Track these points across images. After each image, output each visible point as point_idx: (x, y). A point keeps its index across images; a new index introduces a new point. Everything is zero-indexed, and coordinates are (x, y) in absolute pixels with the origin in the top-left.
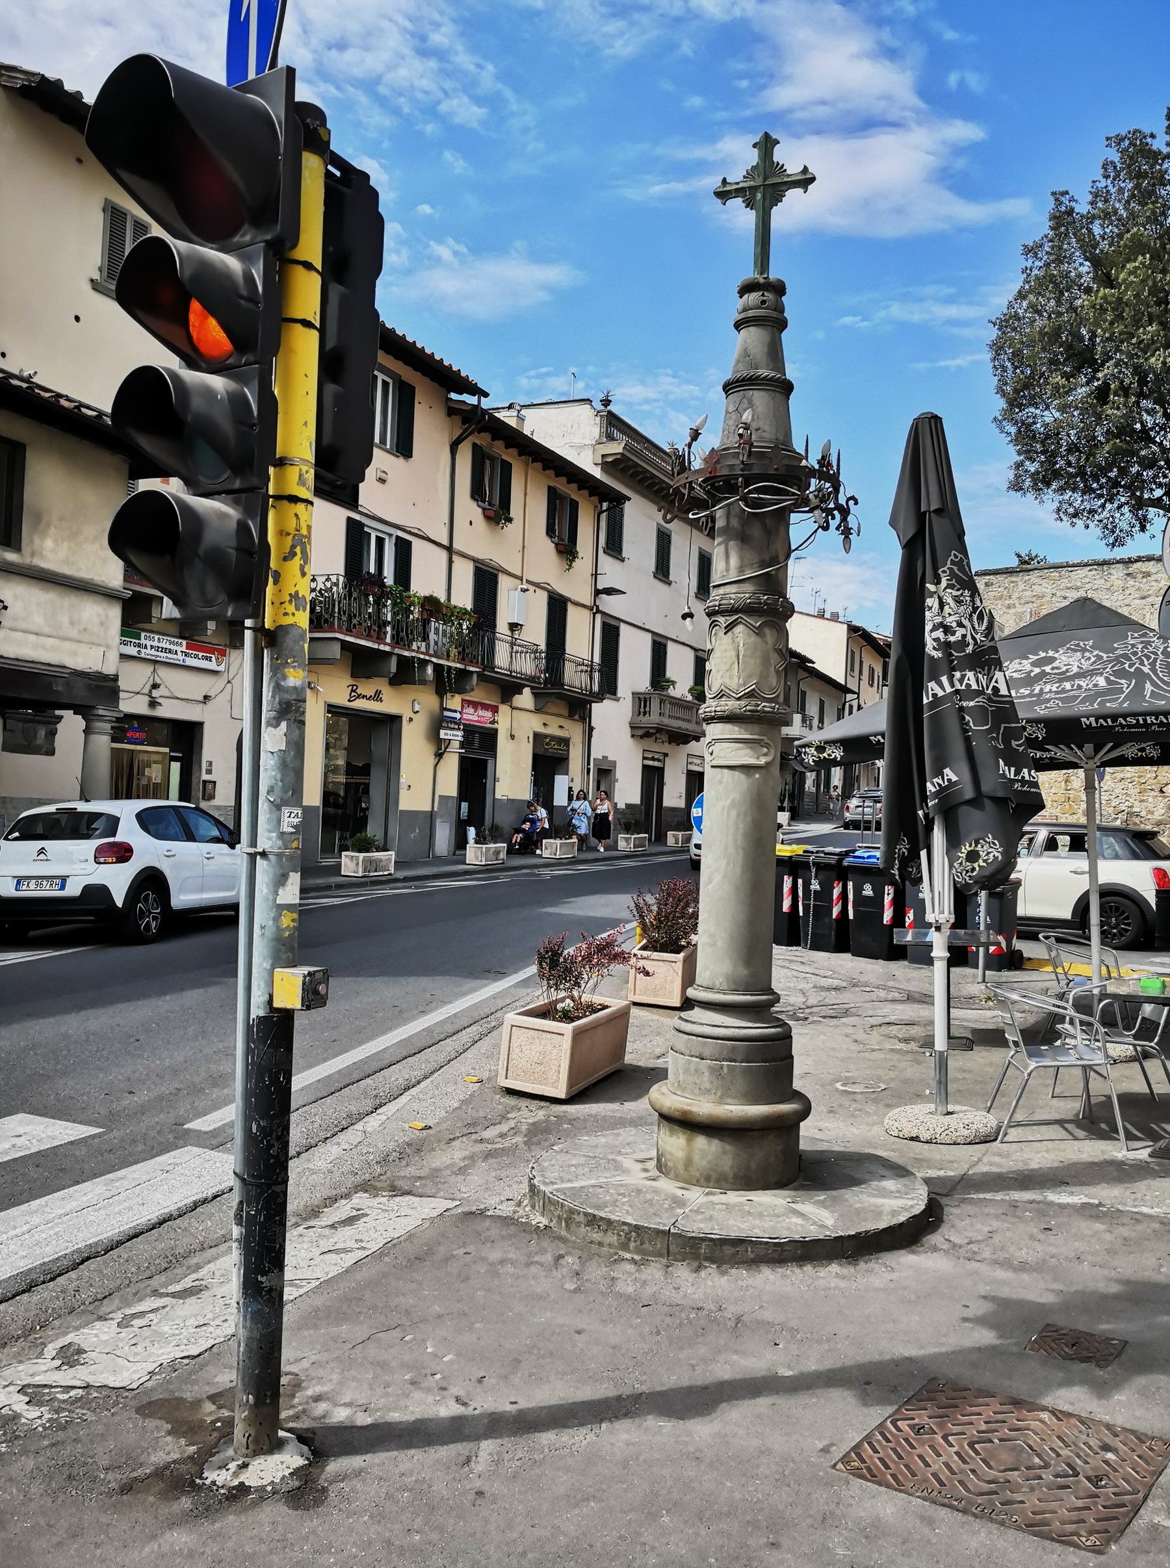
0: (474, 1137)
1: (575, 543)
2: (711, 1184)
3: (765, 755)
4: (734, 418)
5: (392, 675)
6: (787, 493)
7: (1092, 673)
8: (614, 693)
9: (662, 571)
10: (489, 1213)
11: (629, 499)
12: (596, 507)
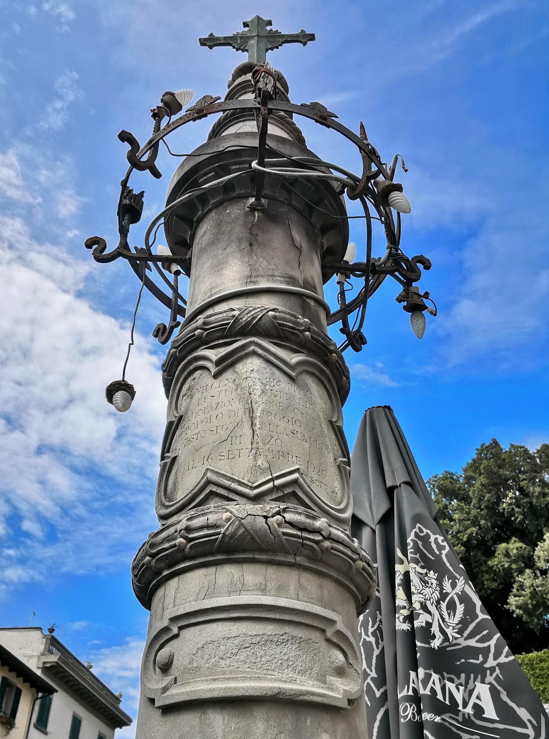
12: (33, 695)
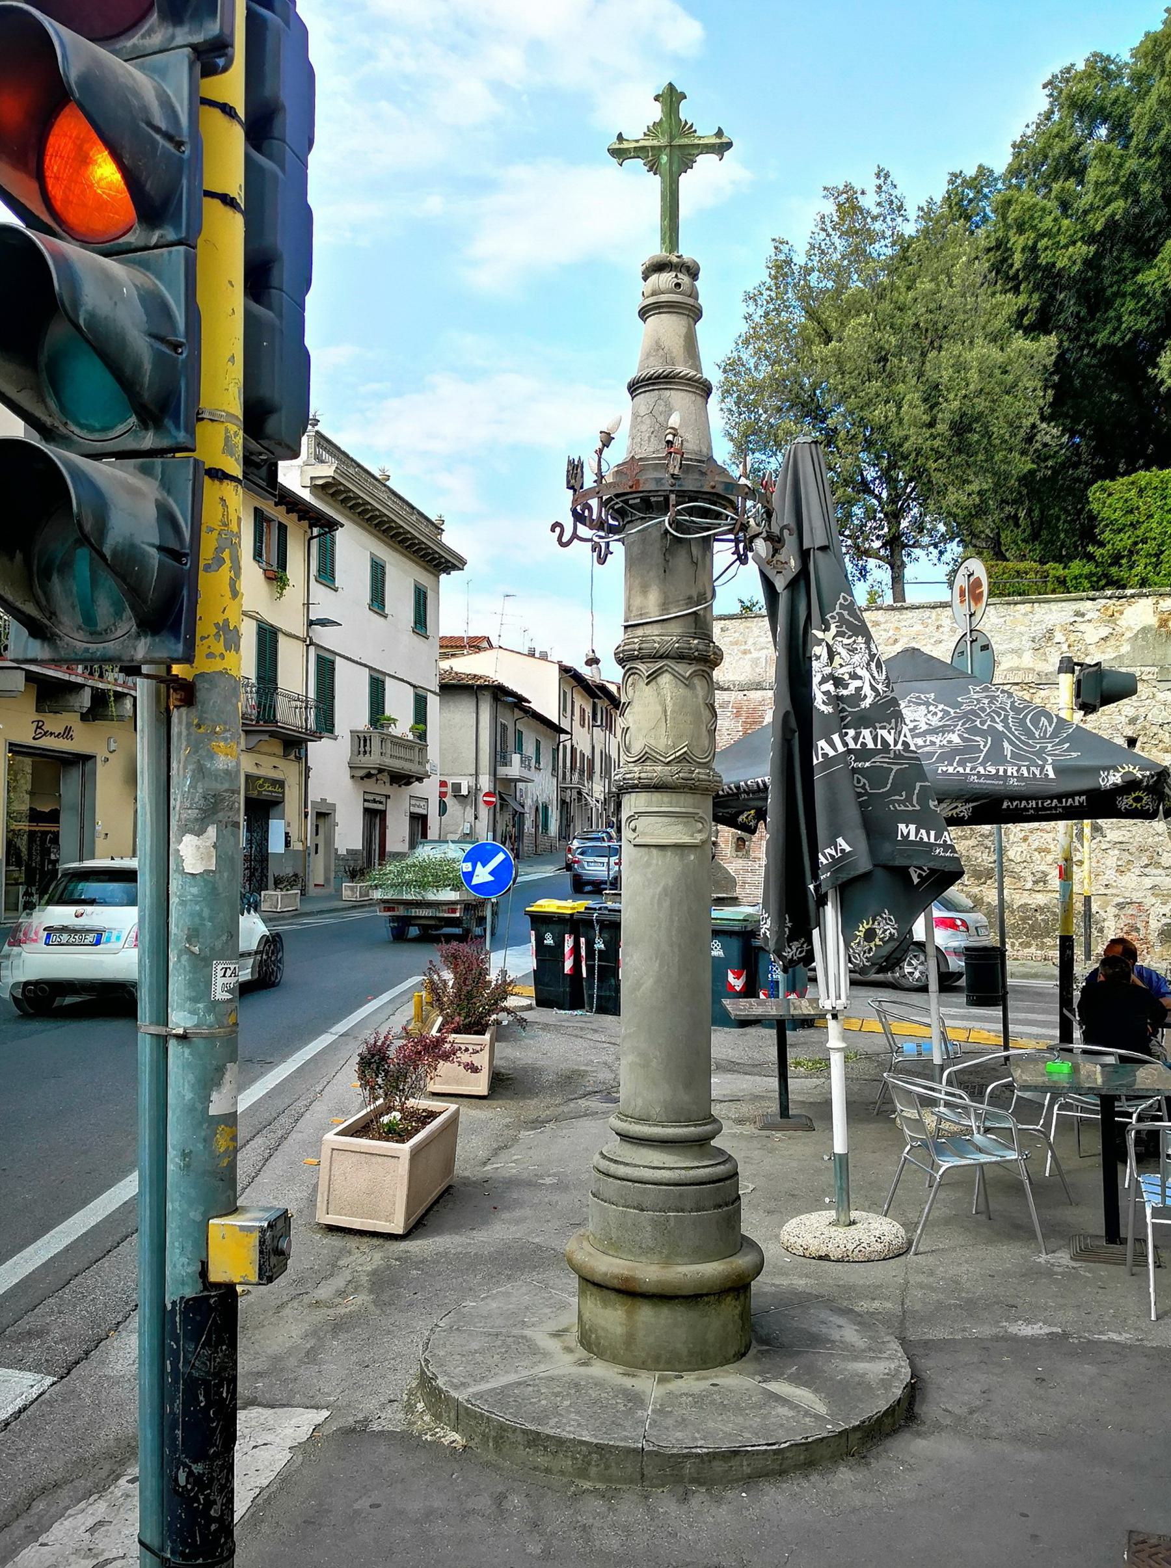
0: (306, 1299)
1: (284, 569)
2: (661, 1366)
3: (700, 831)
4: (648, 422)
5: (85, 710)
6: (718, 515)
7: (942, 730)
8: (332, 731)
9: (378, 600)
10: (375, 1427)
11: (342, 526)
